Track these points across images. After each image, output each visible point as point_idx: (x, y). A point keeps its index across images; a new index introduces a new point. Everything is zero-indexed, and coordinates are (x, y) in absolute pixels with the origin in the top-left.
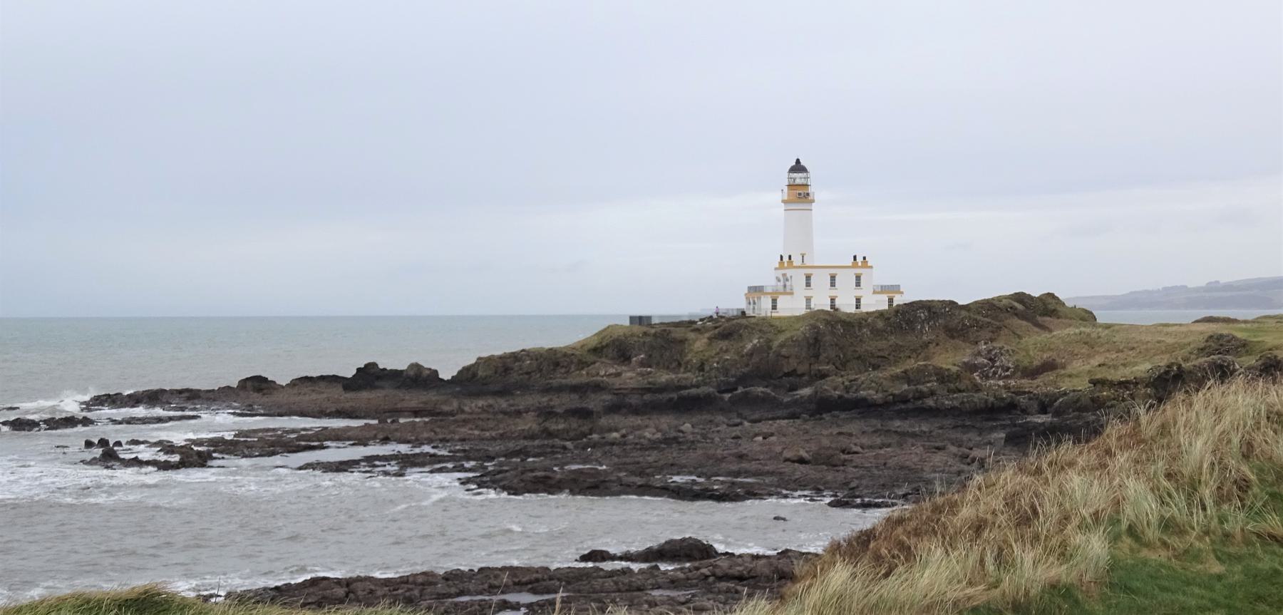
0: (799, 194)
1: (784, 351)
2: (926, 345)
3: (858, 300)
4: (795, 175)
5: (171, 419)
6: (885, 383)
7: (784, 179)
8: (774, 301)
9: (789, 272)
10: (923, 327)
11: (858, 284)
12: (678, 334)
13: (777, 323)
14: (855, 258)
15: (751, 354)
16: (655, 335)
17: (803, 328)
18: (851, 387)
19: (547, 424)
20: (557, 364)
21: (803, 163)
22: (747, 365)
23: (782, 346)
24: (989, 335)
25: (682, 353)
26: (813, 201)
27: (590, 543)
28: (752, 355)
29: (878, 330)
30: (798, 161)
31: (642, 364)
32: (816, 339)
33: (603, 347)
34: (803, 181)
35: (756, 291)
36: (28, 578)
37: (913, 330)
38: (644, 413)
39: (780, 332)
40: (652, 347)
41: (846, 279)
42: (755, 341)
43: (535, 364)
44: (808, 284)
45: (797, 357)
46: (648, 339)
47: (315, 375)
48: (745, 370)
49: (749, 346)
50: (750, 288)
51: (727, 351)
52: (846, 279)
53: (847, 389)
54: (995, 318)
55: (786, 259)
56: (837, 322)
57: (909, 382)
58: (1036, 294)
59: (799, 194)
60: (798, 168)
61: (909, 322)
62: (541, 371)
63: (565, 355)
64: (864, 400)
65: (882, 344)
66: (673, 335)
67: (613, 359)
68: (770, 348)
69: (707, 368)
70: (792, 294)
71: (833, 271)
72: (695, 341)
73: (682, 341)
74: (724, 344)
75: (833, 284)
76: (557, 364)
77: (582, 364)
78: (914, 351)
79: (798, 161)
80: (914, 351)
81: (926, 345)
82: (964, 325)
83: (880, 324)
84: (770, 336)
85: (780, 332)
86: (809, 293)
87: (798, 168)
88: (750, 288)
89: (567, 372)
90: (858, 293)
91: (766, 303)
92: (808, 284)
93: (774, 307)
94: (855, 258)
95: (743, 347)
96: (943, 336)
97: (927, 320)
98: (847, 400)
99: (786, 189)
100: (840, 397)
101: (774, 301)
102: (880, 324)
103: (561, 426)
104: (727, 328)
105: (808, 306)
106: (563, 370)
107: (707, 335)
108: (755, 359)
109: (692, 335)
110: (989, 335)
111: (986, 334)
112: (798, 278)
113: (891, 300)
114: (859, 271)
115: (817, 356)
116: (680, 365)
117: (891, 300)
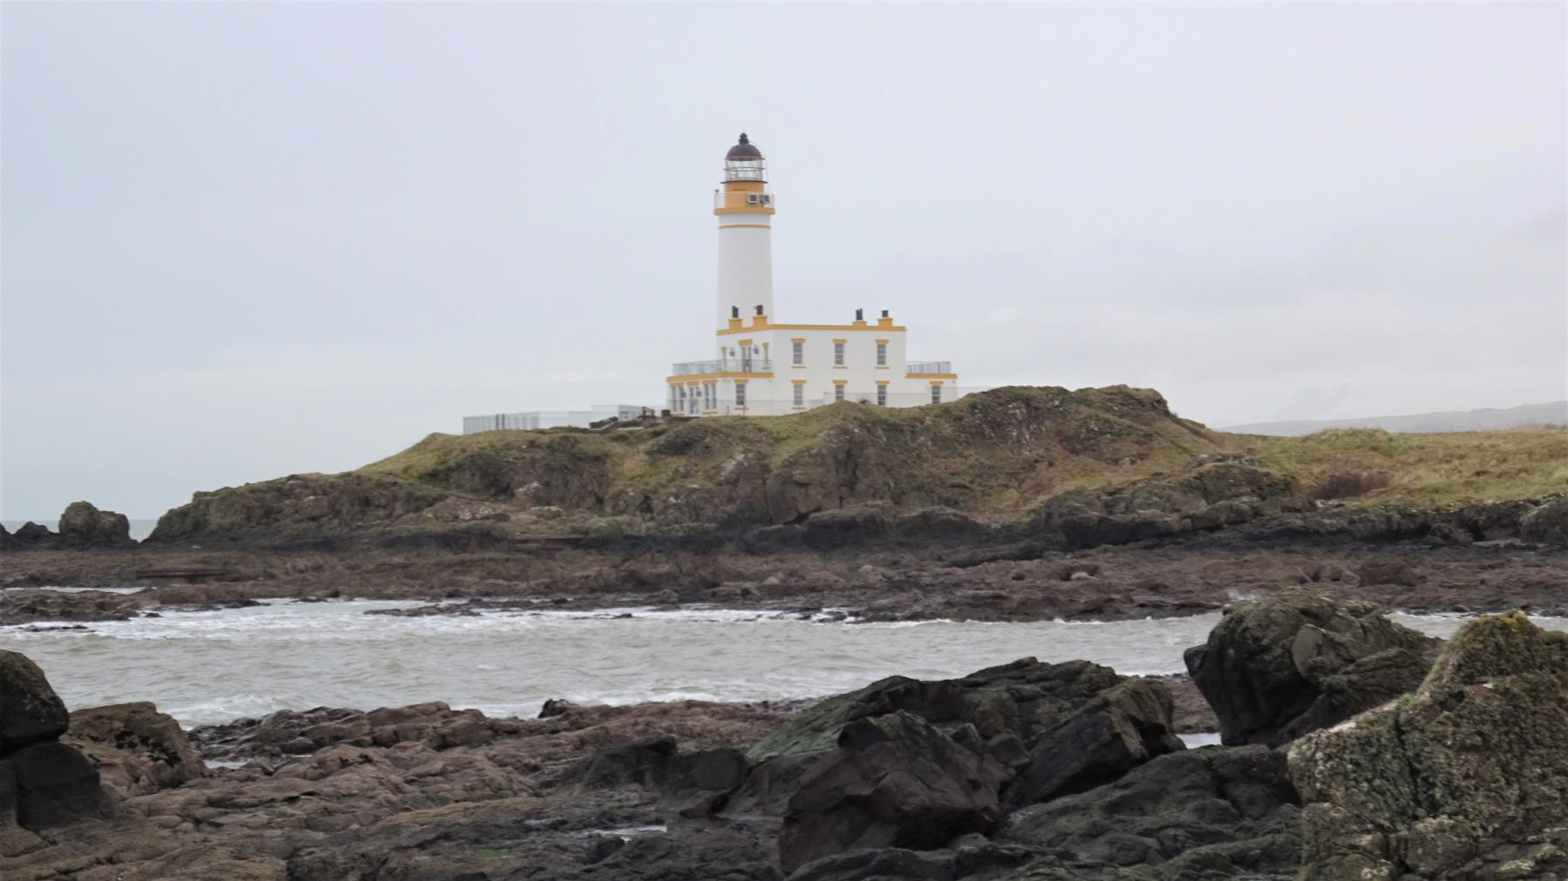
0: (747, 197)
1: (798, 473)
2: (1031, 465)
4: (737, 164)
5: (248, 541)
6: (1176, 495)
7: (715, 170)
8: (741, 389)
9: (758, 338)
10: (1021, 434)
12: (591, 446)
13: (770, 426)
14: (735, 311)
15: (734, 482)
16: (550, 446)
17: (820, 439)
18: (1116, 502)
19: (632, 565)
20: (366, 502)
21: (753, 141)
22: (730, 500)
23: (791, 463)
24: (1135, 449)
25: (602, 479)
26: (772, 212)
28: (736, 481)
29: (944, 439)
31: (537, 499)
32: (848, 453)
33: (449, 470)
34: (751, 175)
37: (1005, 439)
38: (765, 552)
39: (778, 440)
40: (550, 469)
41: (861, 348)
42: (740, 457)
43: (325, 501)
44: (798, 359)
45: (822, 485)
46: (539, 454)
47: (1181, 416)
48: (730, 508)
49: (730, 466)
51: (686, 476)
52: (861, 348)
53: (1109, 507)
54: (1136, 418)
55: (747, 316)
56: (874, 423)
57: (1206, 494)
58: (101, 509)
59: (747, 197)
60: (744, 151)
61: (998, 426)
62: (337, 514)
63: (380, 485)
64: (1149, 524)
65: (957, 463)
66: (581, 446)
67: (474, 490)
68: (766, 469)
69: (656, 504)
70: (770, 375)
71: (798, 334)
72: (622, 457)
73: (600, 459)
74: (679, 463)
75: (839, 359)
76: (366, 502)
77: (417, 503)
78: (1013, 475)
80: (1013, 475)
81: (1031, 465)
82: (1089, 430)
83: (947, 429)
84: (765, 449)
85: (778, 440)
86: (799, 375)
87: (744, 151)
89: (389, 516)
90: (883, 376)
91: (725, 392)
92: (798, 359)
95: (718, 468)
96: (1057, 450)
98: (1117, 526)
99: (722, 188)
100: (1102, 521)
101: (741, 389)
102: (947, 429)
103: (665, 568)
104: (675, 437)
105: (936, 399)
106: (381, 513)
107: (642, 447)
108: (744, 489)
109: (617, 448)
110: (1135, 449)
111: (1128, 447)
113: (936, 390)
115: (851, 484)
116: (600, 501)
117: (936, 390)
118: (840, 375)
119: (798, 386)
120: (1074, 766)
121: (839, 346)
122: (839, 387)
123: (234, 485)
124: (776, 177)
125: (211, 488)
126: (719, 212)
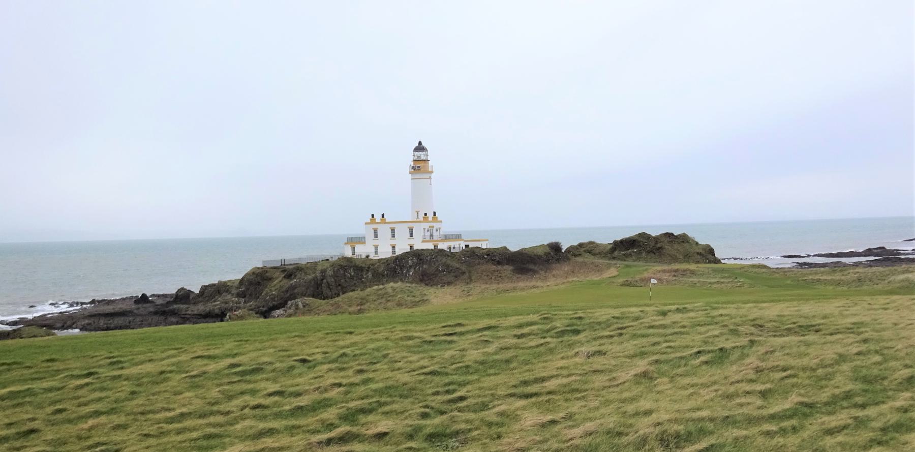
0: (420, 167)
3: (394, 247)
7: (409, 157)
11: (411, 235)
14: (373, 216)
21: (424, 144)
26: (432, 172)
27: (92, 294)
30: (420, 143)
35: (354, 241)
36: (352, 330)
44: (376, 236)
50: (364, 243)
58: (654, 235)
59: (420, 167)
60: (420, 148)
79: (420, 143)
86: (376, 242)
87: (420, 148)
88: (364, 243)
93: (376, 253)
94: (373, 216)
97: (414, 266)
101: (353, 249)
105: (394, 252)
112: (384, 231)
114: (375, 226)
118: (393, 242)
119: (394, 247)
120: (632, 352)
121: (411, 230)
122: (411, 247)
123: (598, 242)
124: (433, 157)
125: (619, 239)
126: (410, 173)
